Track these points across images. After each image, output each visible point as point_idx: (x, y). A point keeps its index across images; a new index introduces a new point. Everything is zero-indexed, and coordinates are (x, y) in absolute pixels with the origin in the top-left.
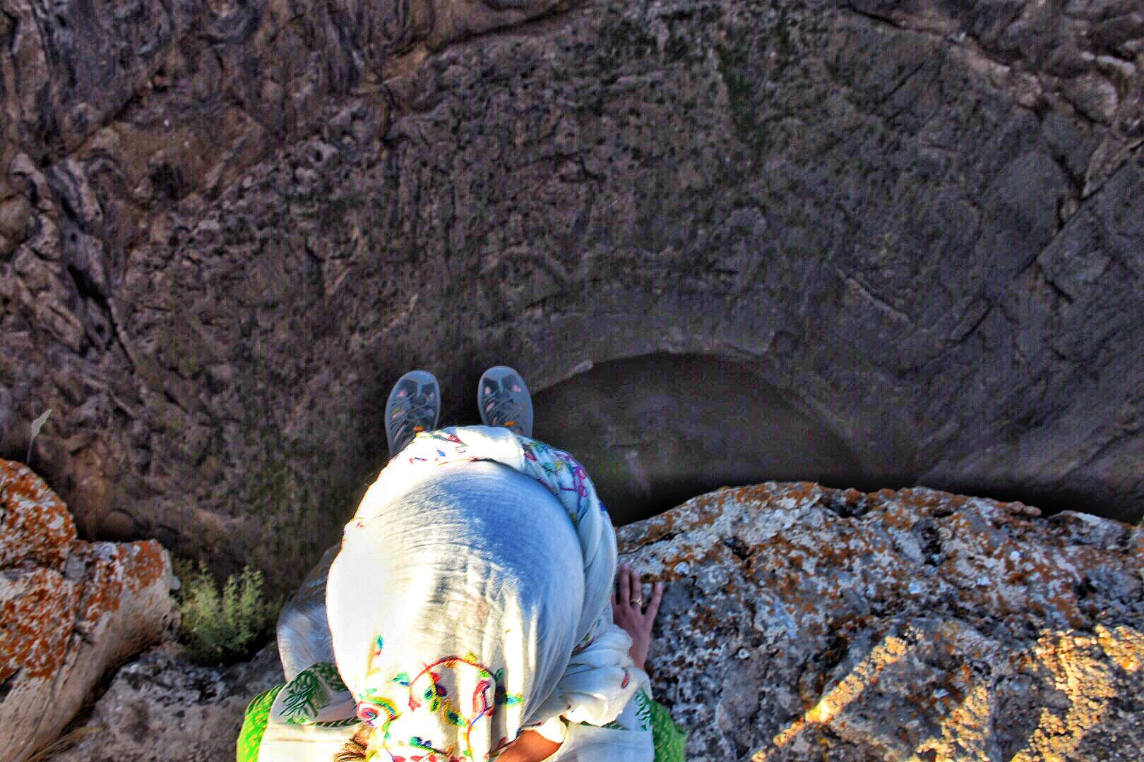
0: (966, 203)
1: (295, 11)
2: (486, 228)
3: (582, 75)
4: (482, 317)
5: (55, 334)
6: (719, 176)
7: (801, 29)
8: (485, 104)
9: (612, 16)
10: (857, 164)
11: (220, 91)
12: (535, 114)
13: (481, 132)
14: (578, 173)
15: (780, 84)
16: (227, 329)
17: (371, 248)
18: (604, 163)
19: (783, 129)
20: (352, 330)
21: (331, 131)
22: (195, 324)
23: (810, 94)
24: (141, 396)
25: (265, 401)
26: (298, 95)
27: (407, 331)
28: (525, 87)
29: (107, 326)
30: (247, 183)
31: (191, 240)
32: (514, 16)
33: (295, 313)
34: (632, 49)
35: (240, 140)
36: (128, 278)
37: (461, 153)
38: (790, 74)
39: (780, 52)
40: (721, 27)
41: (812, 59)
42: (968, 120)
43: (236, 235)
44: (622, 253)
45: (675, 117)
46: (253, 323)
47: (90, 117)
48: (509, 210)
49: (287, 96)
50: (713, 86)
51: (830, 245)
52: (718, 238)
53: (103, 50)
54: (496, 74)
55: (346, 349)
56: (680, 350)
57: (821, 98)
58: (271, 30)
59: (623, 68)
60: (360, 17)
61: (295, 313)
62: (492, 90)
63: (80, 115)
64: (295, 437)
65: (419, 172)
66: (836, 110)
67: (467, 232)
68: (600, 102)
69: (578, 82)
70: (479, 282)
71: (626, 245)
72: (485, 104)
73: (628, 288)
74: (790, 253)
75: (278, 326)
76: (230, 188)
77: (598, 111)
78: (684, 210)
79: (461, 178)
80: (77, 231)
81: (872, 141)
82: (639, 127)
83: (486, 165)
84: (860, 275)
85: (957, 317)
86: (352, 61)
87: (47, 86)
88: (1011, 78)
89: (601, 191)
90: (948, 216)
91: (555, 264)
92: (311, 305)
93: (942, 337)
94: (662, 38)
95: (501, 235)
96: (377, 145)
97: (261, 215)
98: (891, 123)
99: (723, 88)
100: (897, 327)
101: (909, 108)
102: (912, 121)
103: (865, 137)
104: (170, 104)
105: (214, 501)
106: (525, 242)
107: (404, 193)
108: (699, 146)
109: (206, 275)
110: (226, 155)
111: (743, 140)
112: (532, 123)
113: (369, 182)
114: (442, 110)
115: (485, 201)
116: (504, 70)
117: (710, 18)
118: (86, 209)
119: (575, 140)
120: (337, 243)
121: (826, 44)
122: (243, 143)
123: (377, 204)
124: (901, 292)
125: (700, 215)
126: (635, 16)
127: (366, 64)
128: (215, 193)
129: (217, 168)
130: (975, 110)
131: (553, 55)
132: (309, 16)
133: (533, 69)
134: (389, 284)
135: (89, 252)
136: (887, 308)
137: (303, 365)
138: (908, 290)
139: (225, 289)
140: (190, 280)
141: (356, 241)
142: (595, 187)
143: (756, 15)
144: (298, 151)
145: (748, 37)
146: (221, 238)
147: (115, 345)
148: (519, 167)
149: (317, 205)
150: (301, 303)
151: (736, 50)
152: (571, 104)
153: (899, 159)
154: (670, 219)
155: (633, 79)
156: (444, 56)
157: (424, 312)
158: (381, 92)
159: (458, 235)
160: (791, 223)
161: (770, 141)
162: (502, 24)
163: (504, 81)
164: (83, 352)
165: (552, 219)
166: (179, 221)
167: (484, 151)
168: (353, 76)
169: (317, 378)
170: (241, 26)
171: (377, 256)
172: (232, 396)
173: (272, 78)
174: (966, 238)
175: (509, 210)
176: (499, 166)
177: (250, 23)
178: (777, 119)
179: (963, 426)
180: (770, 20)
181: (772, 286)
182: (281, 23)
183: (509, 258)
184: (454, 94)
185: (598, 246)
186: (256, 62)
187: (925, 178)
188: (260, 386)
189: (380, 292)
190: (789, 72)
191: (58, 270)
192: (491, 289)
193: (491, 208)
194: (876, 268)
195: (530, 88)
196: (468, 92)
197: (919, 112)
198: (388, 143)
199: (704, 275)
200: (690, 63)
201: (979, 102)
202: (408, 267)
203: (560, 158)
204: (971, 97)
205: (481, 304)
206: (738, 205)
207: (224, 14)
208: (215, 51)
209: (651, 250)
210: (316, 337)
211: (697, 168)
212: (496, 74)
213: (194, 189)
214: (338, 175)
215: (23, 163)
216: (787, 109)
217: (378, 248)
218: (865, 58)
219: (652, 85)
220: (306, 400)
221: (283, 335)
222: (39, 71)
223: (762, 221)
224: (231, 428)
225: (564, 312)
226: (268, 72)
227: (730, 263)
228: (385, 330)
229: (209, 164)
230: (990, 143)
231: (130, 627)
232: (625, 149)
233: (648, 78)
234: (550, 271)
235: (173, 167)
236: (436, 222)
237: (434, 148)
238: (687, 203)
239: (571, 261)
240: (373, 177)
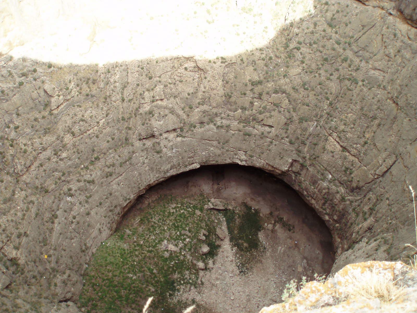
56: (244, 163)
84: (335, 135)
89: (205, 78)
91: (181, 112)
93: (373, 172)
124: (355, 146)
130: (399, 51)
141: (72, 90)
142: (202, 75)
179: (377, 221)
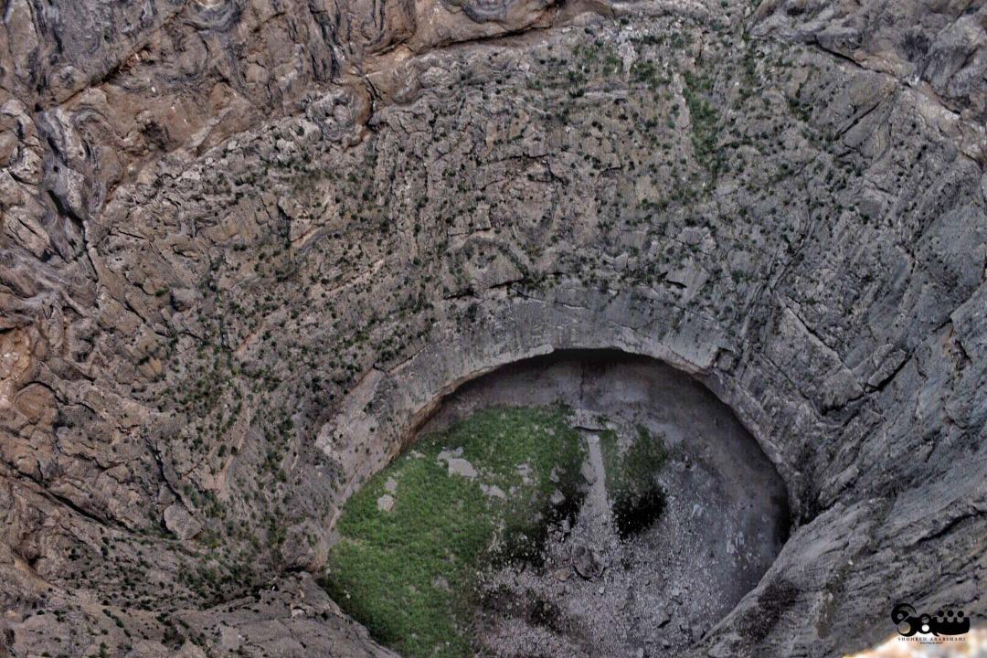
0: (902, 250)
1: (276, 9)
2: (455, 212)
3: (553, 86)
4: (446, 290)
5: (18, 240)
6: (675, 192)
7: (767, 61)
8: (460, 103)
9: (587, 36)
10: (805, 198)
11: (205, 68)
12: (505, 117)
13: (454, 128)
14: (545, 174)
15: (740, 112)
16: (198, 261)
17: (342, 215)
18: (568, 168)
19: (739, 156)
20: (314, 280)
21: (315, 112)
22: (168, 254)
23: (768, 126)
24: (98, 301)
25: (222, 326)
26: (283, 79)
27: (369, 290)
28: (498, 92)
29: (79, 241)
30: (231, 146)
31: (173, 186)
32: (492, 29)
33: (261, 258)
34: (601, 67)
35: (227, 110)
36: (108, 207)
37: (435, 144)
38: (750, 104)
39: (743, 82)
40: (689, 54)
41: (773, 92)
42: (912, 166)
43: (213, 188)
44: (582, 252)
45: (636, 133)
46: (222, 260)
47: (76, 78)
48: (478, 199)
49: (273, 79)
50: (675, 108)
51: (773, 273)
52: (671, 251)
53: (88, 27)
54: (473, 78)
55: (305, 295)
57: (778, 130)
58: (254, 23)
59: (589, 84)
60: (338, 18)
61: (261, 258)
62: (468, 91)
63: (68, 76)
64: (246, 359)
65: (396, 155)
66: (789, 144)
67: (438, 214)
68: (566, 112)
69: (548, 92)
70: (445, 258)
71: (587, 245)
72: (460, 103)
73: (585, 284)
74: (736, 276)
75: (243, 266)
76: (214, 148)
77: (564, 121)
78: (640, 222)
79: (435, 167)
80: (60, 165)
81: (821, 178)
82: (599, 139)
83: (458, 157)
85: (877, 362)
86: (333, 55)
87: (36, 53)
88: (958, 127)
90: (883, 261)
91: (520, 254)
92: (276, 254)
93: (862, 380)
94: (628, 61)
95: (468, 220)
96: (359, 128)
97: (239, 173)
98: (840, 160)
99: (685, 112)
100: (827, 364)
101: (858, 148)
102: (859, 161)
103: (815, 172)
104: (157, 74)
105: (147, 395)
106: (493, 230)
107: (381, 172)
108: (656, 164)
109: (182, 215)
110: (213, 121)
111: (701, 162)
112: (503, 125)
113: (348, 157)
114: (422, 105)
115: (456, 188)
116: (481, 75)
117: (680, 45)
118: (68, 149)
119: (541, 145)
120: (307, 205)
121: (789, 78)
122: (229, 113)
123: (353, 178)
125: (655, 228)
126: (608, 38)
127: (346, 59)
128: (200, 151)
129: (204, 131)
130: (920, 156)
131: (528, 66)
132: (290, 14)
133: (508, 77)
134: (356, 247)
135: (69, 184)
136: (819, 343)
137: (262, 301)
138: (839, 329)
139: (198, 229)
140: (167, 217)
143: (728, 45)
144: (282, 125)
145: (716, 66)
146: (200, 187)
147: (83, 259)
148: (489, 162)
149: (293, 171)
150: (268, 251)
151: (705, 77)
152: (541, 112)
153: (843, 198)
154: (626, 227)
155: (599, 95)
156: (425, 58)
157: (389, 276)
158: (363, 83)
159: (428, 214)
160: (739, 247)
161: (727, 166)
162: (482, 35)
164: (46, 257)
165: (520, 212)
166: (166, 170)
167: (457, 145)
168: (335, 67)
169: (275, 314)
170: (225, 18)
171: (347, 222)
172: (191, 316)
173: (257, 62)
174: (897, 285)
175: (478, 199)
176: (471, 159)
177: (233, 15)
178: (735, 146)
180: (738, 51)
181: (716, 304)
182: (263, 19)
183: (476, 241)
184: (434, 92)
185: (562, 243)
186: (240, 48)
187: (866, 219)
188: (219, 312)
189: (345, 253)
190: (750, 103)
191: (35, 192)
192: (457, 265)
193: (461, 195)
194: (812, 302)
195: (502, 95)
196: (447, 91)
197: (867, 154)
198: (370, 127)
199: (655, 283)
200: (655, 84)
201: (924, 148)
202: (378, 236)
203: (527, 159)
204: (919, 143)
205: (448, 280)
206: (690, 223)
207: (208, 7)
208: (200, 36)
209: (610, 254)
210: (279, 280)
211: (654, 183)
212: (473, 78)
213: (181, 145)
214: (319, 149)
215: (13, 107)
216: (746, 137)
217: (348, 215)
218: (824, 94)
219: (617, 102)
220: (261, 332)
221: (247, 273)
222: (30, 38)
223: (711, 241)
224: (186, 341)
225: (526, 298)
226: (253, 57)
227: (679, 276)
228: (348, 285)
229: (196, 127)
230: (930, 192)
231: (794, 582)
232: (587, 158)
233: (614, 95)
234: (514, 260)
235: (161, 125)
236: (408, 201)
237: (412, 136)
238: (643, 215)
239: (535, 253)
240: (353, 155)
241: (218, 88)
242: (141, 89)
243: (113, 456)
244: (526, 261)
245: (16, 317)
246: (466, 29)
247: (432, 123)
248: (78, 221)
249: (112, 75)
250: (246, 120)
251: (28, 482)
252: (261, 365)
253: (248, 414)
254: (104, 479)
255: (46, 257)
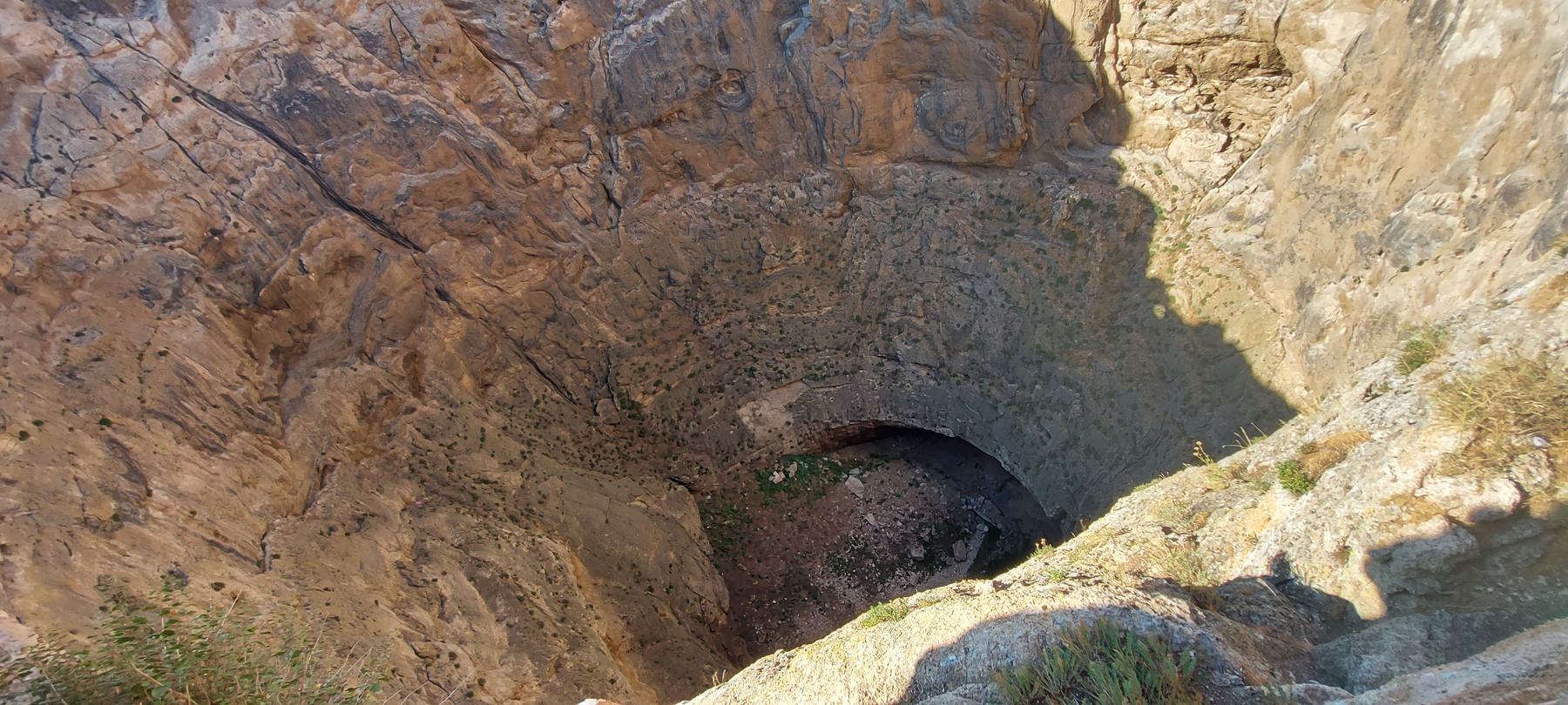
20: (772, 302)
32: (957, 158)
44: (988, 367)
48: (916, 291)
50: (1086, 275)
91: (941, 347)
110: (729, 170)
113: (826, 225)
114: (891, 202)
128: (718, 186)
133: (961, 200)
135: (617, 184)
163: (936, 200)
166: (691, 193)
175: (916, 291)
219: (1038, 251)
220: (725, 321)
226: (761, 133)
229: (716, 172)
234: (936, 350)
238: (1035, 358)
241: (735, 149)
242: (677, 137)
243: (579, 353)
244: (944, 356)
245: (544, 250)
246: (936, 152)
247: (894, 219)
248: (618, 207)
249: (657, 123)
250: (754, 175)
251: (510, 342)
252: (716, 342)
253: (690, 368)
254: (568, 363)
255: (585, 222)
